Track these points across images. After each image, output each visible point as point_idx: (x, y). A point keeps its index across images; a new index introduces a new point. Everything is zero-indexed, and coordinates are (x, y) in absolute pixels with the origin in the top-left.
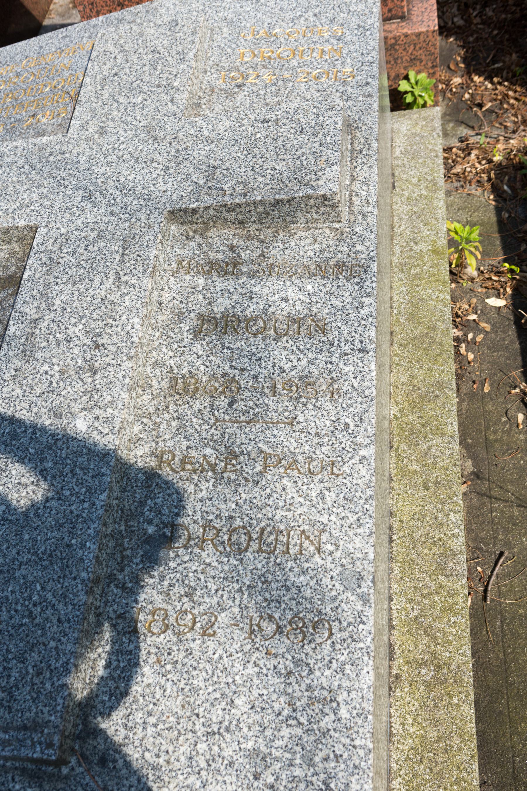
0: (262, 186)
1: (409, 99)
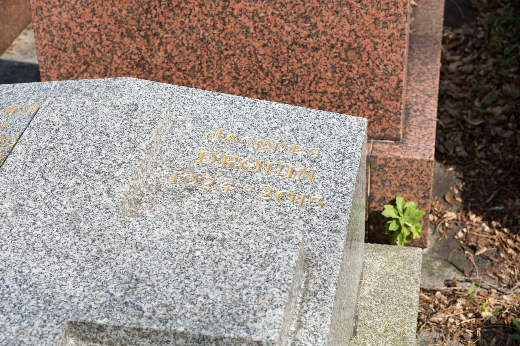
0: (188, 315)
1: (393, 227)
